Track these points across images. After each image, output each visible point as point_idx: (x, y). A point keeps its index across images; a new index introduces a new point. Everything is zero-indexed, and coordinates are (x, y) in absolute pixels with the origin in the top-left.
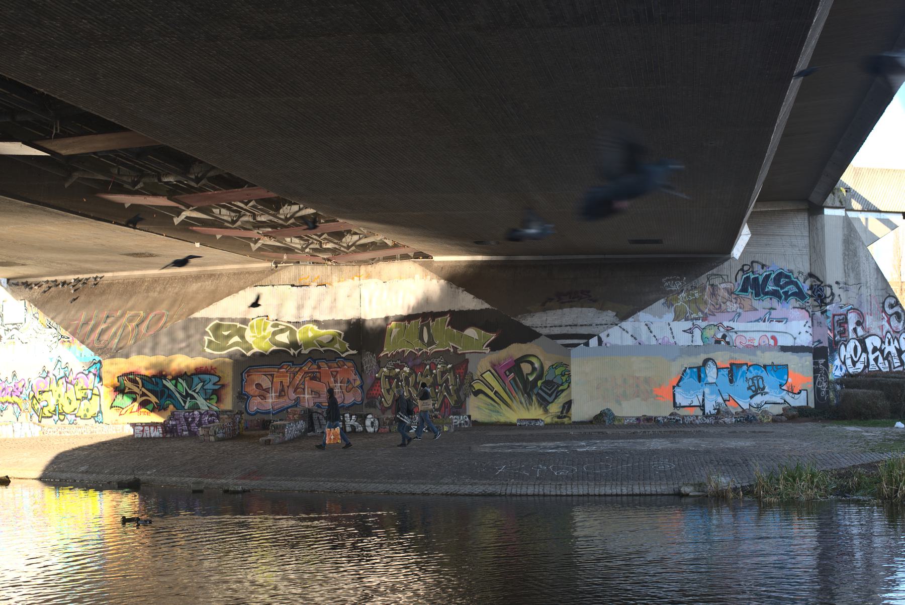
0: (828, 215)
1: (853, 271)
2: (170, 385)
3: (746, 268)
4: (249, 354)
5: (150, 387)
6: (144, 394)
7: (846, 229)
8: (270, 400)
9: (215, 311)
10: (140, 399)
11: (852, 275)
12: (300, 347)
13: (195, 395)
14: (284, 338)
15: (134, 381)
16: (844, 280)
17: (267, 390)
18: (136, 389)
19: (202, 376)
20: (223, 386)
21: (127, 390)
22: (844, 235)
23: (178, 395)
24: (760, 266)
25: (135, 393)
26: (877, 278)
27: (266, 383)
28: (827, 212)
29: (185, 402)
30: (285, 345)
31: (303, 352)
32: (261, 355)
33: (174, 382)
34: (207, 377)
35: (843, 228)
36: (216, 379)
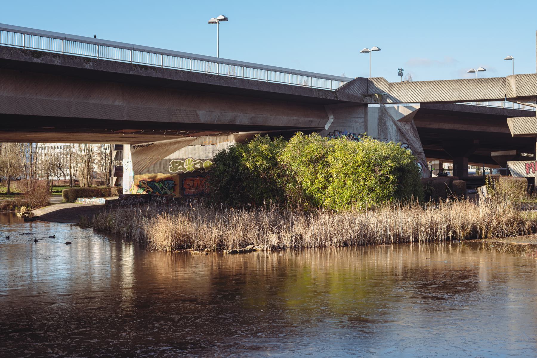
0: (370, 107)
1: (383, 133)
2: (157, 185)
3: (331, 134)
4: (185, 172)
5: (150, 185)
6: (148, 188)
7: (380, 113)
8: (193, 190)
9: (174, 156)
10: (146, 190)
11: (383, 134)
12: (204, 169)
13: (166, 188)
14: (198, 166)
15: (144, 183)
16: (378, 137)
17: (192, 187)
18: (145, 186)
19: (168, 181)
20: (176, 185)
21: (142, 187)
22: (379, 116)
23: (160, 188)
24: (339, 132)
25: (145, 188)
26: (397, 135)
27: (191, 184)
28: (370, 106)
29: (162, 191)
30: (198, 169)
31: (205, 171)
32: (189, 173)
33: (158, 183)
34: (170, 182)
35: (378, 113)
36: (173, 182)
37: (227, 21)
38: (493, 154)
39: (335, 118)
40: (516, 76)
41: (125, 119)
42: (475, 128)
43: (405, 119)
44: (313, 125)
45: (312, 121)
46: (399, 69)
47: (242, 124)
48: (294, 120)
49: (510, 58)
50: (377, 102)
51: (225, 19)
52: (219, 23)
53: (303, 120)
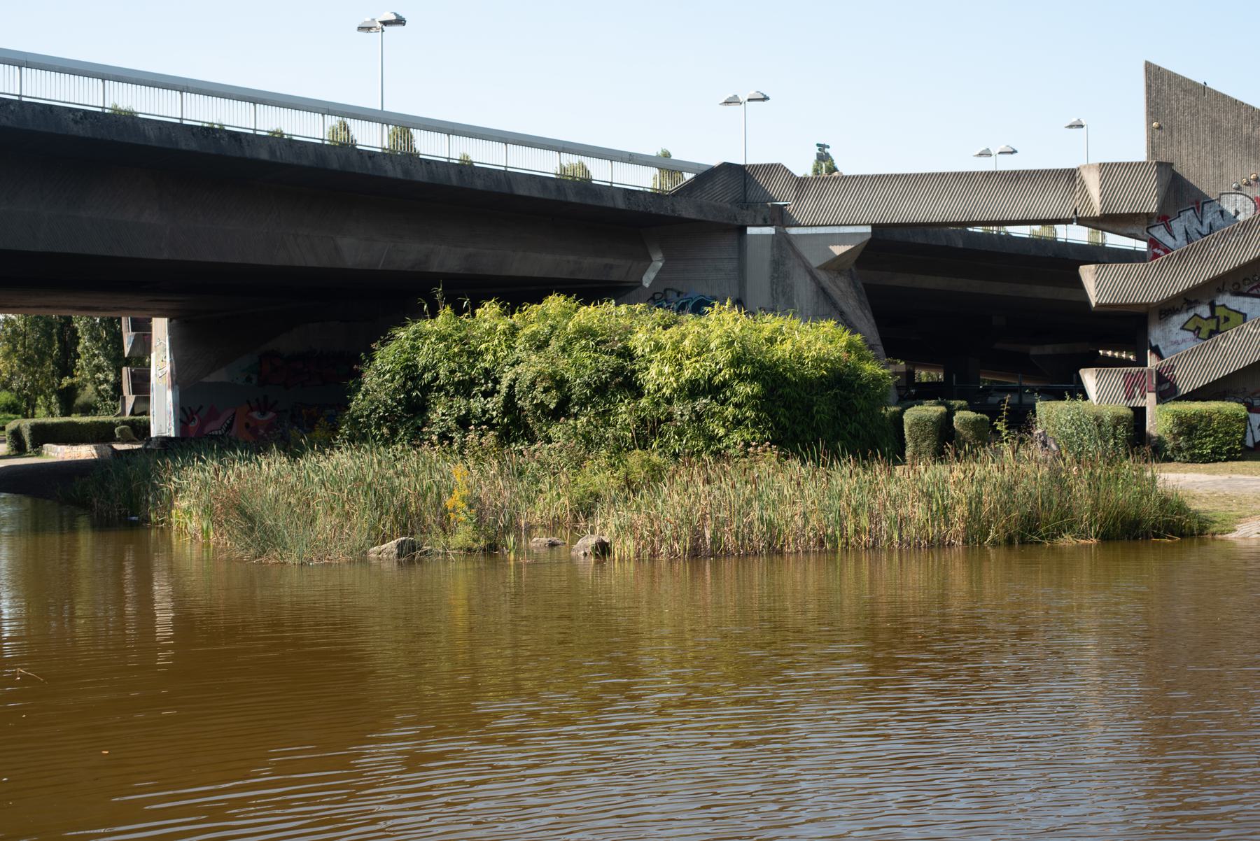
0: (752, 235)
1: (784, 296)
3: (657, 297)
24: (675, 294)
28: (751, 231)
37: (404, 24)
38: (1035, 351)
39: (667, 259)
40: (1103, 166)
41: (165, 255)
42: (998, 288)
43: (835, 266)
44: (615, 276)
45: (611, 267)
46: (818, 145)
47: (443, 270)
48: (568, 262)
49: (1079, 124)
50: (768, 223)
51: (399, 21)
52: (383, 31)
53: (589, 265)
